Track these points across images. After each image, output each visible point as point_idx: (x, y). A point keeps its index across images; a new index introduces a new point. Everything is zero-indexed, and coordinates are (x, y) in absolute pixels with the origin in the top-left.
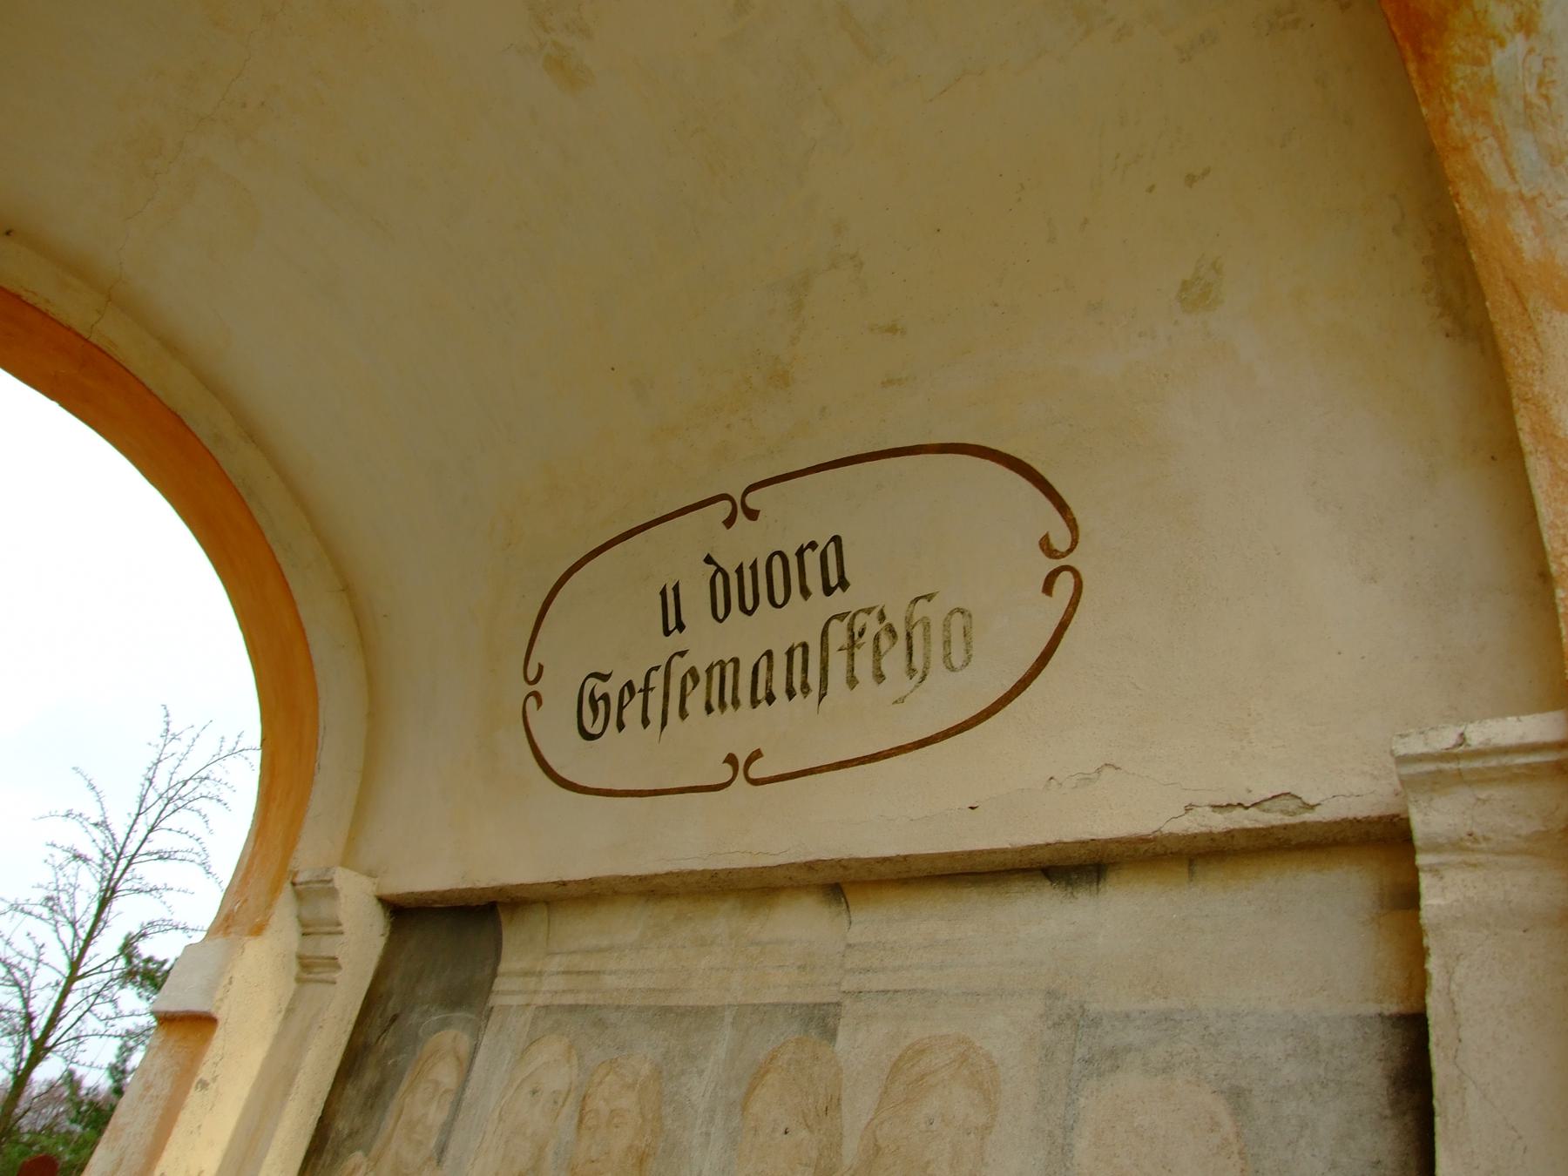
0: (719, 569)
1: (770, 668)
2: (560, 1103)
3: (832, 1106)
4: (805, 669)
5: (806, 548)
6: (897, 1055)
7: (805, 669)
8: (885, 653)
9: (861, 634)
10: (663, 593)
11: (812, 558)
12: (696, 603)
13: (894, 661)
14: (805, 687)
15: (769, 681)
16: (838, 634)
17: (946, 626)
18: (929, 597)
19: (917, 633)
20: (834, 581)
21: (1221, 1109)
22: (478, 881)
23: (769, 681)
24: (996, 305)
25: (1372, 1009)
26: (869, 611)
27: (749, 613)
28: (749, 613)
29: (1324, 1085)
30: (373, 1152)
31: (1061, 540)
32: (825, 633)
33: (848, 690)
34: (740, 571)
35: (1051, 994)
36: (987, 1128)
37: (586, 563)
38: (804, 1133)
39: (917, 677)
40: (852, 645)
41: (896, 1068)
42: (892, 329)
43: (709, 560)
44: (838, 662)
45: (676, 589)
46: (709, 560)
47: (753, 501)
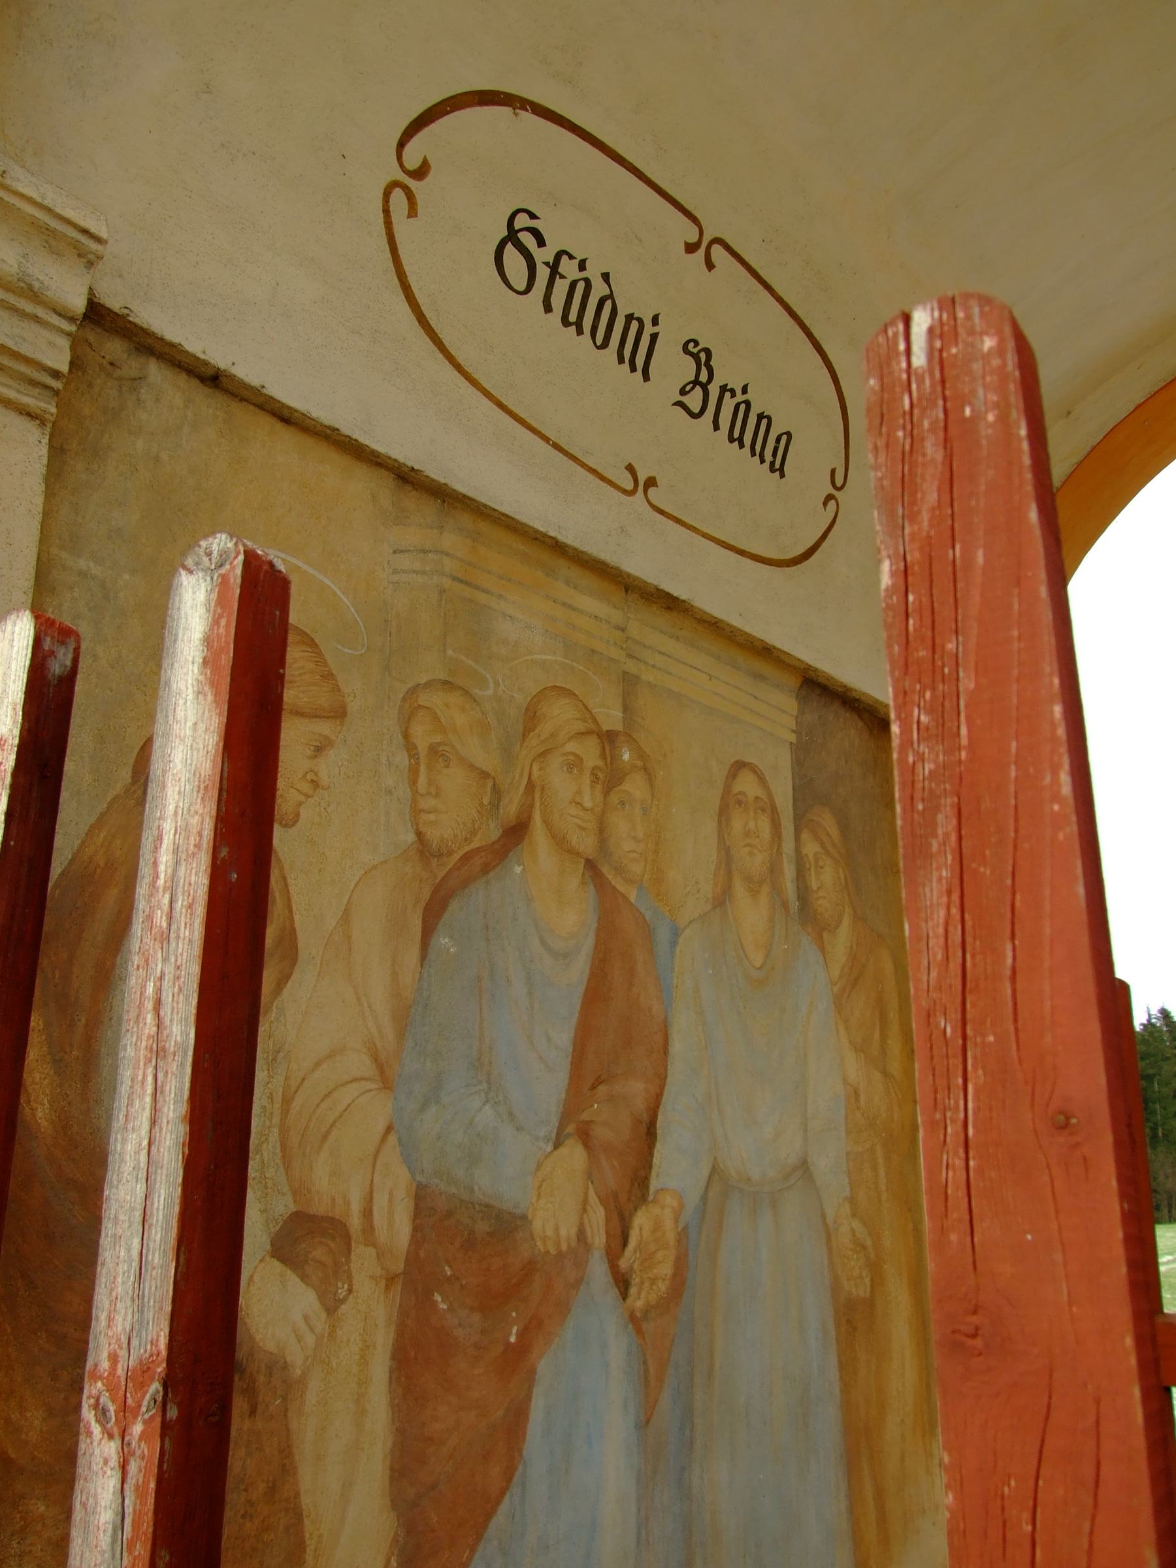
47: (717, 252)
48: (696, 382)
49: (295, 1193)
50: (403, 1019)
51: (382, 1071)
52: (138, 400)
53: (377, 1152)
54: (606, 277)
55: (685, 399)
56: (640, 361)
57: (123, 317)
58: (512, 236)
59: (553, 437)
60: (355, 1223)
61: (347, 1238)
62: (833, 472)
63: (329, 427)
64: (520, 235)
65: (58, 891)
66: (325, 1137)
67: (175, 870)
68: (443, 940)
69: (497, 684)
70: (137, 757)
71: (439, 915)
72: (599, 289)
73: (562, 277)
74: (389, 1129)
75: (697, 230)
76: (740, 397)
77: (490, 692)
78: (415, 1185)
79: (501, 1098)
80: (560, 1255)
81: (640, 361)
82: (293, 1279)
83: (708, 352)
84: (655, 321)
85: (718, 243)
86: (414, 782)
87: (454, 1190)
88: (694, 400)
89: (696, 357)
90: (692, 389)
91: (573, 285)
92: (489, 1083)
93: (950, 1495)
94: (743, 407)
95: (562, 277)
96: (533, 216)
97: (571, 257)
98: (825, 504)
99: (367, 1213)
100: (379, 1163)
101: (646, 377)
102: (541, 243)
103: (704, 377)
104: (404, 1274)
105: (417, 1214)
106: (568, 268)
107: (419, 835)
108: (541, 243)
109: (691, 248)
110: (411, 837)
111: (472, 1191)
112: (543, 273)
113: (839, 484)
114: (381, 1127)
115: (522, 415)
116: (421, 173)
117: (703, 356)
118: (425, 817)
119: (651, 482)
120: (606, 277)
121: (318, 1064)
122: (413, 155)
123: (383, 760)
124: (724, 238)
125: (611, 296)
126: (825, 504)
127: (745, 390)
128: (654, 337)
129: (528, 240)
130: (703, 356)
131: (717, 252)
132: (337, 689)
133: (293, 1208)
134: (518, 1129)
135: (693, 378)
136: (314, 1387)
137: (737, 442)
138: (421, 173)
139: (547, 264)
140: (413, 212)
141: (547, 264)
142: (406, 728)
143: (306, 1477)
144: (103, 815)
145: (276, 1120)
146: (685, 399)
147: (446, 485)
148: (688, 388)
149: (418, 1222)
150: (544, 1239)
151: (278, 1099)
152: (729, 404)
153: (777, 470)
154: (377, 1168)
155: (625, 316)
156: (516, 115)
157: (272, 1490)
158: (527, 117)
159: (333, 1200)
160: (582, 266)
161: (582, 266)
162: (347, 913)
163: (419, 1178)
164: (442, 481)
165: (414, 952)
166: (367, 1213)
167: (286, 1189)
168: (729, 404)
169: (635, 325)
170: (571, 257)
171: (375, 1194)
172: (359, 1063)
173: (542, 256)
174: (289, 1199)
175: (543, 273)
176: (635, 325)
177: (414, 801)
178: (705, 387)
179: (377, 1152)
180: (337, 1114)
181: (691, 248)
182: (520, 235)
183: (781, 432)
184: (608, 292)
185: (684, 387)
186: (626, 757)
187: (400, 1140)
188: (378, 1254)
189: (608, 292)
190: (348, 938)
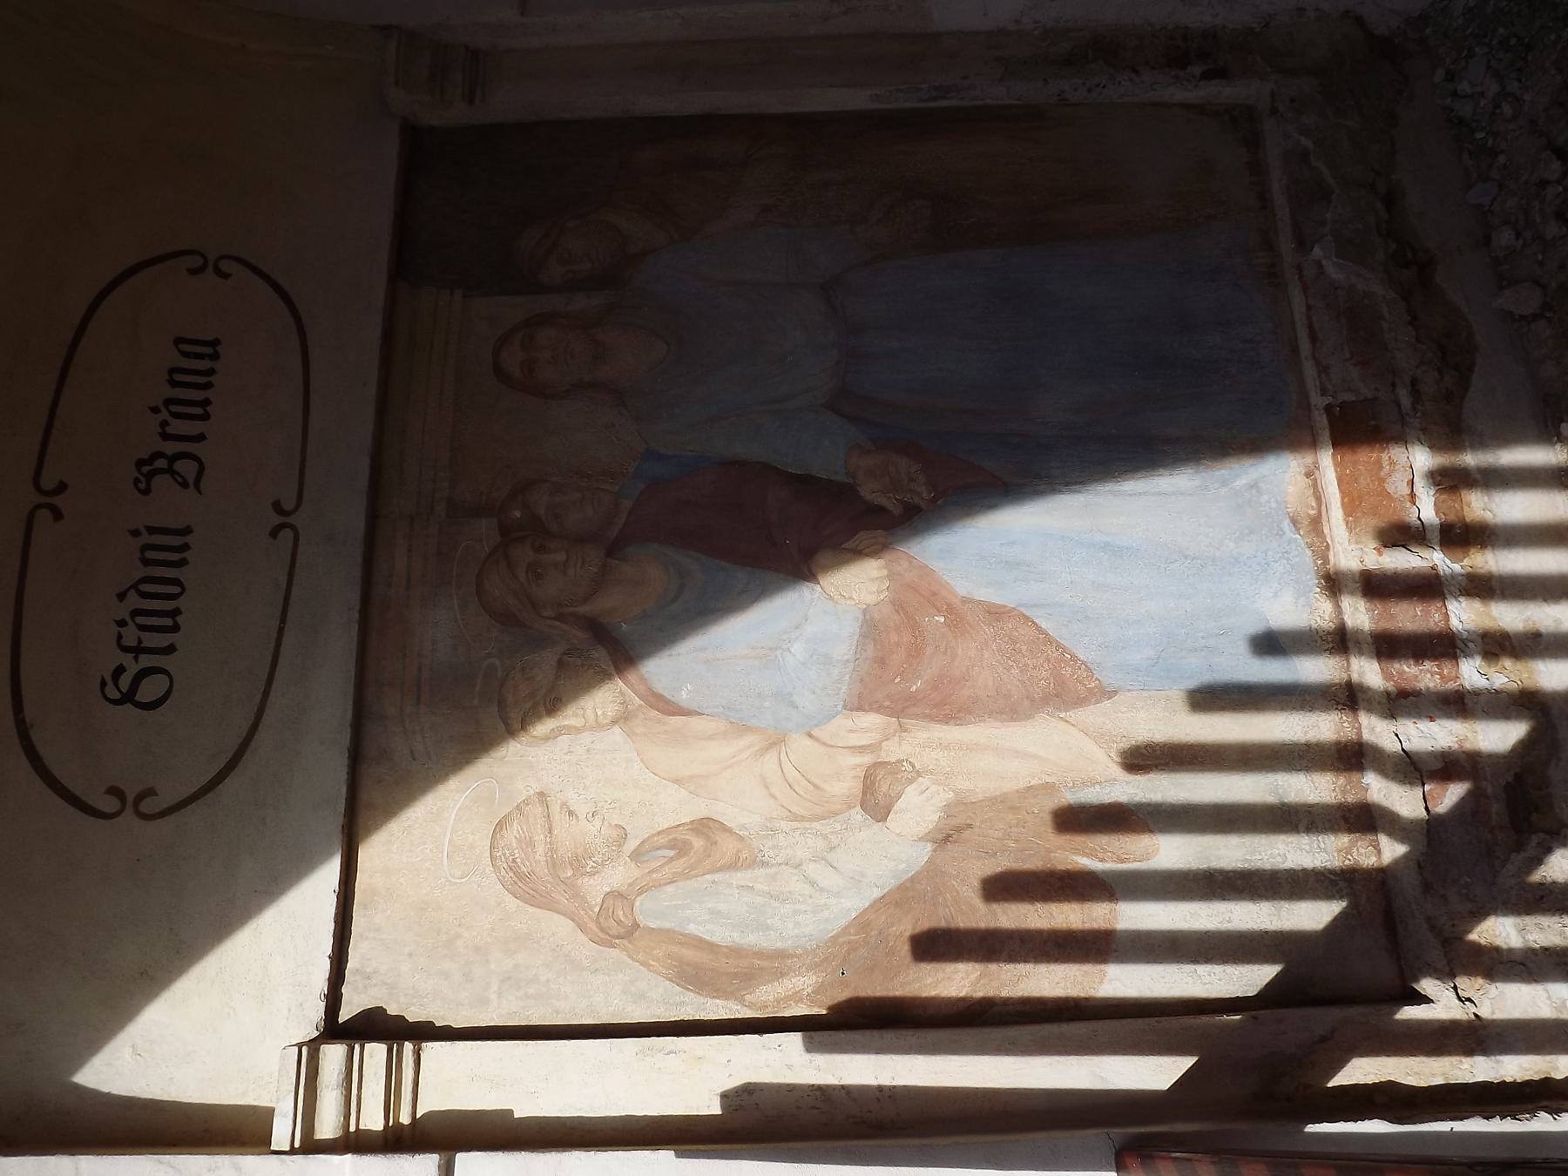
48: (171, 471)
49: (850, 808)
50: (743, 729)
51: (774, 744)
52: (374, 972)
53: (824, 744)
54: (121, 596)
55: (191, 481)
57: (327, 997)
58: (128, 698)
59: (275, 624)
60: (867, 759)
61: (877, 765)
63: (343, 832)
64: (124, 691)
66: (815, 786)
68: (684, 697)
69: (489, 655)
70: (606, 946)
71: (667, 701)
72: (134, 601)
73: (140, 641)
74: (810, 736)
75: (168, 680)
76: (164, 415)
77: (498, 663)
78: (845, 712)
79: (785, 637)
80: (890, 577)
82: (899, 805)
83: (140, 463)
84: (135, 533)
86: (578, 730)
87: (847, 677)
88: (187, 468)
89: (150, 476)
90: (178, 474)
91: (143, 628)
92: (776, 649)
94: (174, 409)
95: (140, 641)
96: (103, 684)
97: (120, 637)
98: (226, 276)
99: (861, 749)
100: (830, 742)
101: (187, 531)
102: (120, 670)
103: (161, 463)
104: (898, 718)
105: (860, 708)
106: (131, 636)
107: (614, 722)
108: (120, 670)
110: (617, 729)
111: (847, 661)
112: (146, 661)
114: (808, 742)
115: (270, 658)
116: (115, 792)
117: (146, 469)
118: (601, 719)
120: (121, 596)
121: (773, 796)
122: (109, 804)
123: (567, 757)
124: (167, 657)
125: (135, 586)
127: (155, 410)
128: (152, 530)
129: (125, 681)
130: (146, 469)
131: (48, 482)
132: (526, 802)
133: (858, 808)
134: (806, 620)
135: (167, 476)
136: (963, 784)
137: (208, 409)
138: (115, 792)
139: (136, 659)
141: (136, 659)
142: (542, 739)
143: (1010, 786)
144: (641, 964)
145: (807, 825)
146: (191, 481)
147: (351, 726)
148: (179, 479)
149: (867, 708)
150: (880, 592)
151: (796, 824)
152: (178, 427)
154: (833, 744)
156: (32, 725)
157: (1013, 809)
158: (30, 713)
159: (854, 777)
160: (122, 623)
161: (122, 623)
162: (677, 781)
163: (840, 708)
164: (349, 730)
165: (694, 720)
166: (861, 749)
167: (847, 814)
168: (178, 427)
169: (151, 555)
170: (120, 637)
171: (850, 745)
172: (769, 763)
173: (133, 668)
174: (853, 811)
175: (146, 661)
176: (151, 555)
177: (592, 728)
178: (173, 459)
179: (824, 744)
180: (803, 778)
181: (57, 515)
182: (124, 690)
183: (177, 352)
184: (133, 591)
185: (180, 484)
186: (518, 514)
187: (816, 726)
188: (886, 740)
189: (133, 591)
190: (691, 777)
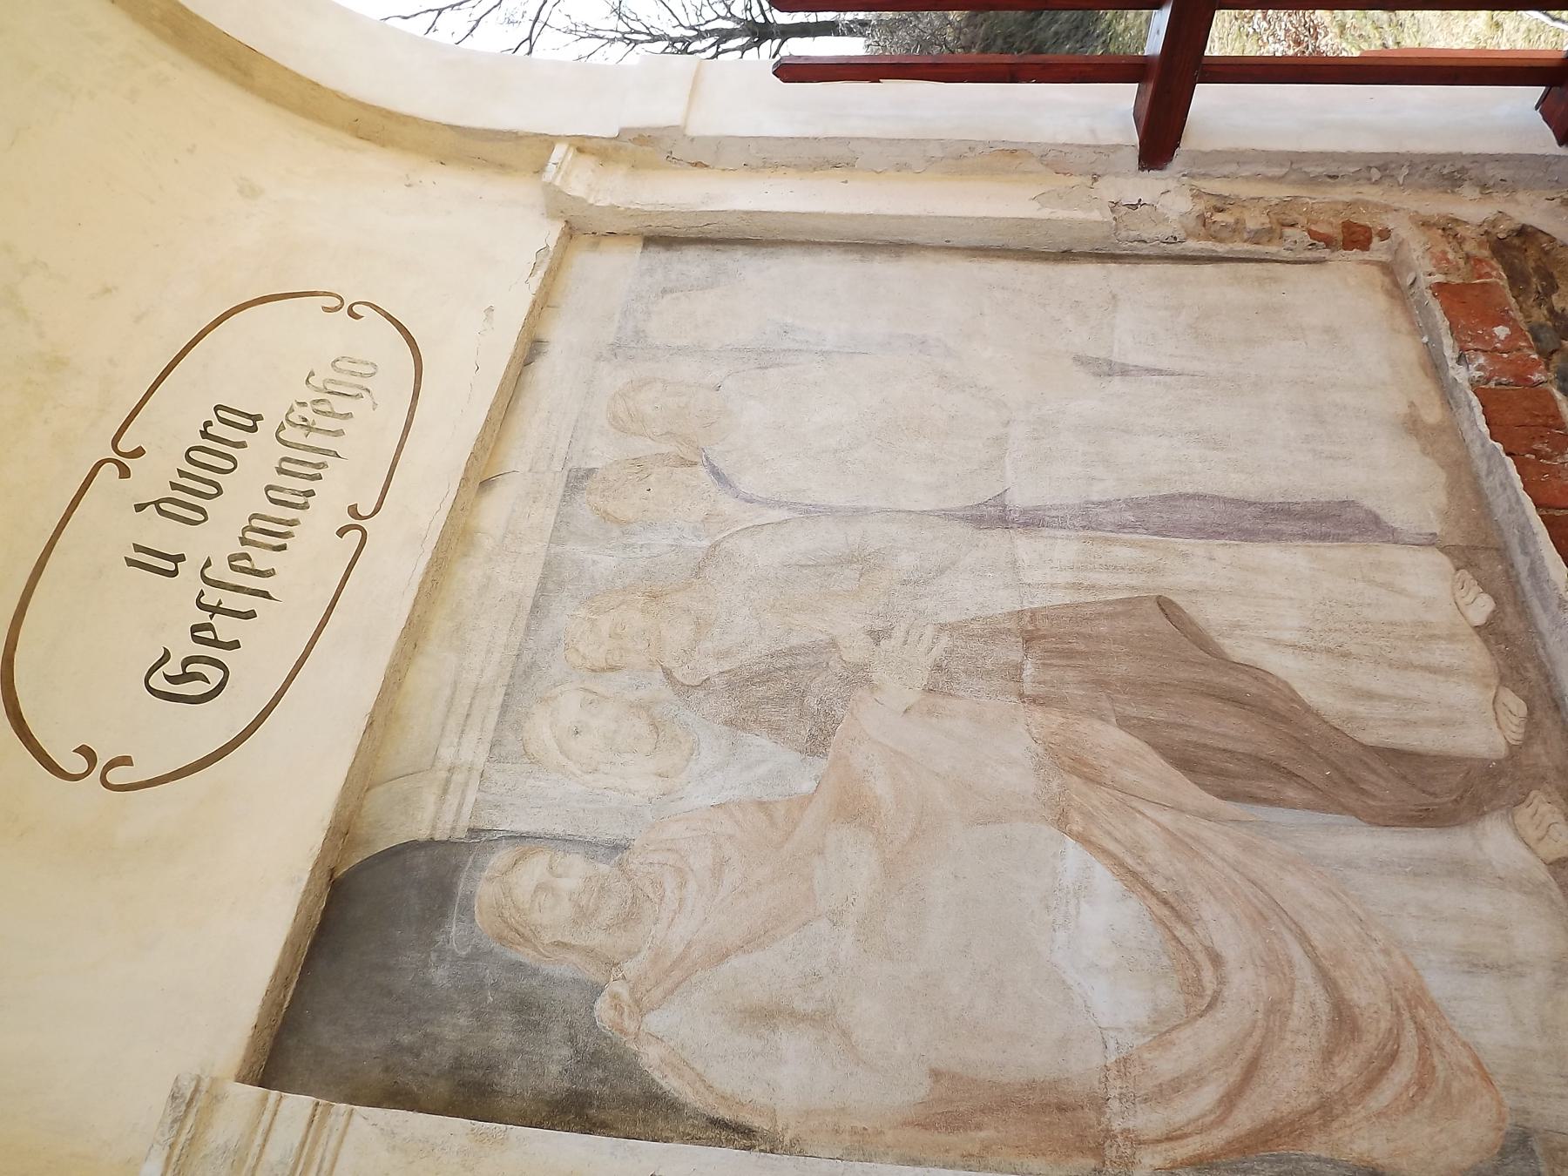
0: (157, 503)
1: (281, 490)
2: (594, 697)
3: (637, 462)
4: (303, 463)
5: (205, 429)
6: (614, 430)
7: (303, 463)
8: (332, 408)
9: (305, 420)
10: (131, 562)
11: (217, 429)
12: (164, 535)
13: (341, 405)
14: (317, 466)
15: (293, 492)
16: (289, 434)
17: (340, 371)
18: (312, 374)
19: (330, 387)
20: (249, 423)
21: (668, 297)
22: (322, 820)
23: (293, 492)
24: (157, 246)
25: (640, 250)
26: (292, 410)
27: (220, 492)
28: (220, 492)
29: (666, 268)
30: (592, 973)
31: (117, 776)
32: (284, 443)
33: (352, 419)
34: (174, 486)
35: (598, 358)
36: (664, 381)
37: (18, 634)
38: (652, 478)
39: (365, 394)
40: (309, 428)
41: (624, 430)
42: (107, 291)
43: (140, 508)
44: (315, 440)
45: (138, 548)
46: (140, 508)
47: (126, 445)
56: (316, 458)
62: (326, 309)
65: (1533, 457)
67: (1154, 893)
81: (316, 458)
85: (116, 447)
93: (1371, 1105)
98: (356, 317)
109: (125, 472)
113: (337, 302)
116: (87, 753)
119: (353, 511)
126: (356, 317)
131: (126, 445)
138: (87, 753)
140: (126, 761)
153: (255, 424)
155: (774, 73)
181: (125, 472)
